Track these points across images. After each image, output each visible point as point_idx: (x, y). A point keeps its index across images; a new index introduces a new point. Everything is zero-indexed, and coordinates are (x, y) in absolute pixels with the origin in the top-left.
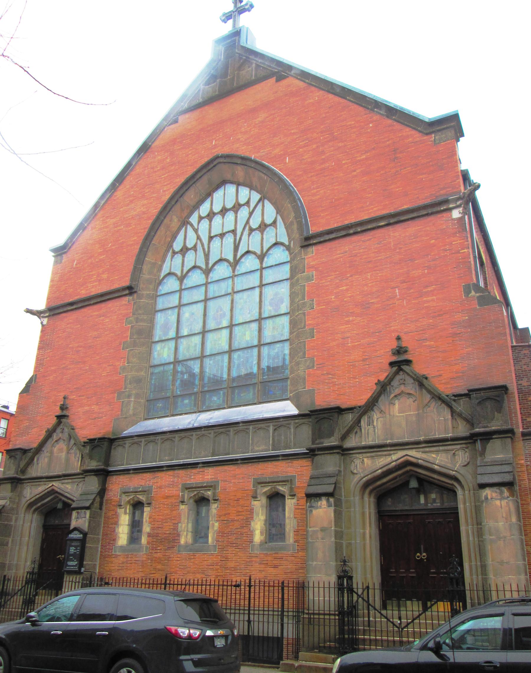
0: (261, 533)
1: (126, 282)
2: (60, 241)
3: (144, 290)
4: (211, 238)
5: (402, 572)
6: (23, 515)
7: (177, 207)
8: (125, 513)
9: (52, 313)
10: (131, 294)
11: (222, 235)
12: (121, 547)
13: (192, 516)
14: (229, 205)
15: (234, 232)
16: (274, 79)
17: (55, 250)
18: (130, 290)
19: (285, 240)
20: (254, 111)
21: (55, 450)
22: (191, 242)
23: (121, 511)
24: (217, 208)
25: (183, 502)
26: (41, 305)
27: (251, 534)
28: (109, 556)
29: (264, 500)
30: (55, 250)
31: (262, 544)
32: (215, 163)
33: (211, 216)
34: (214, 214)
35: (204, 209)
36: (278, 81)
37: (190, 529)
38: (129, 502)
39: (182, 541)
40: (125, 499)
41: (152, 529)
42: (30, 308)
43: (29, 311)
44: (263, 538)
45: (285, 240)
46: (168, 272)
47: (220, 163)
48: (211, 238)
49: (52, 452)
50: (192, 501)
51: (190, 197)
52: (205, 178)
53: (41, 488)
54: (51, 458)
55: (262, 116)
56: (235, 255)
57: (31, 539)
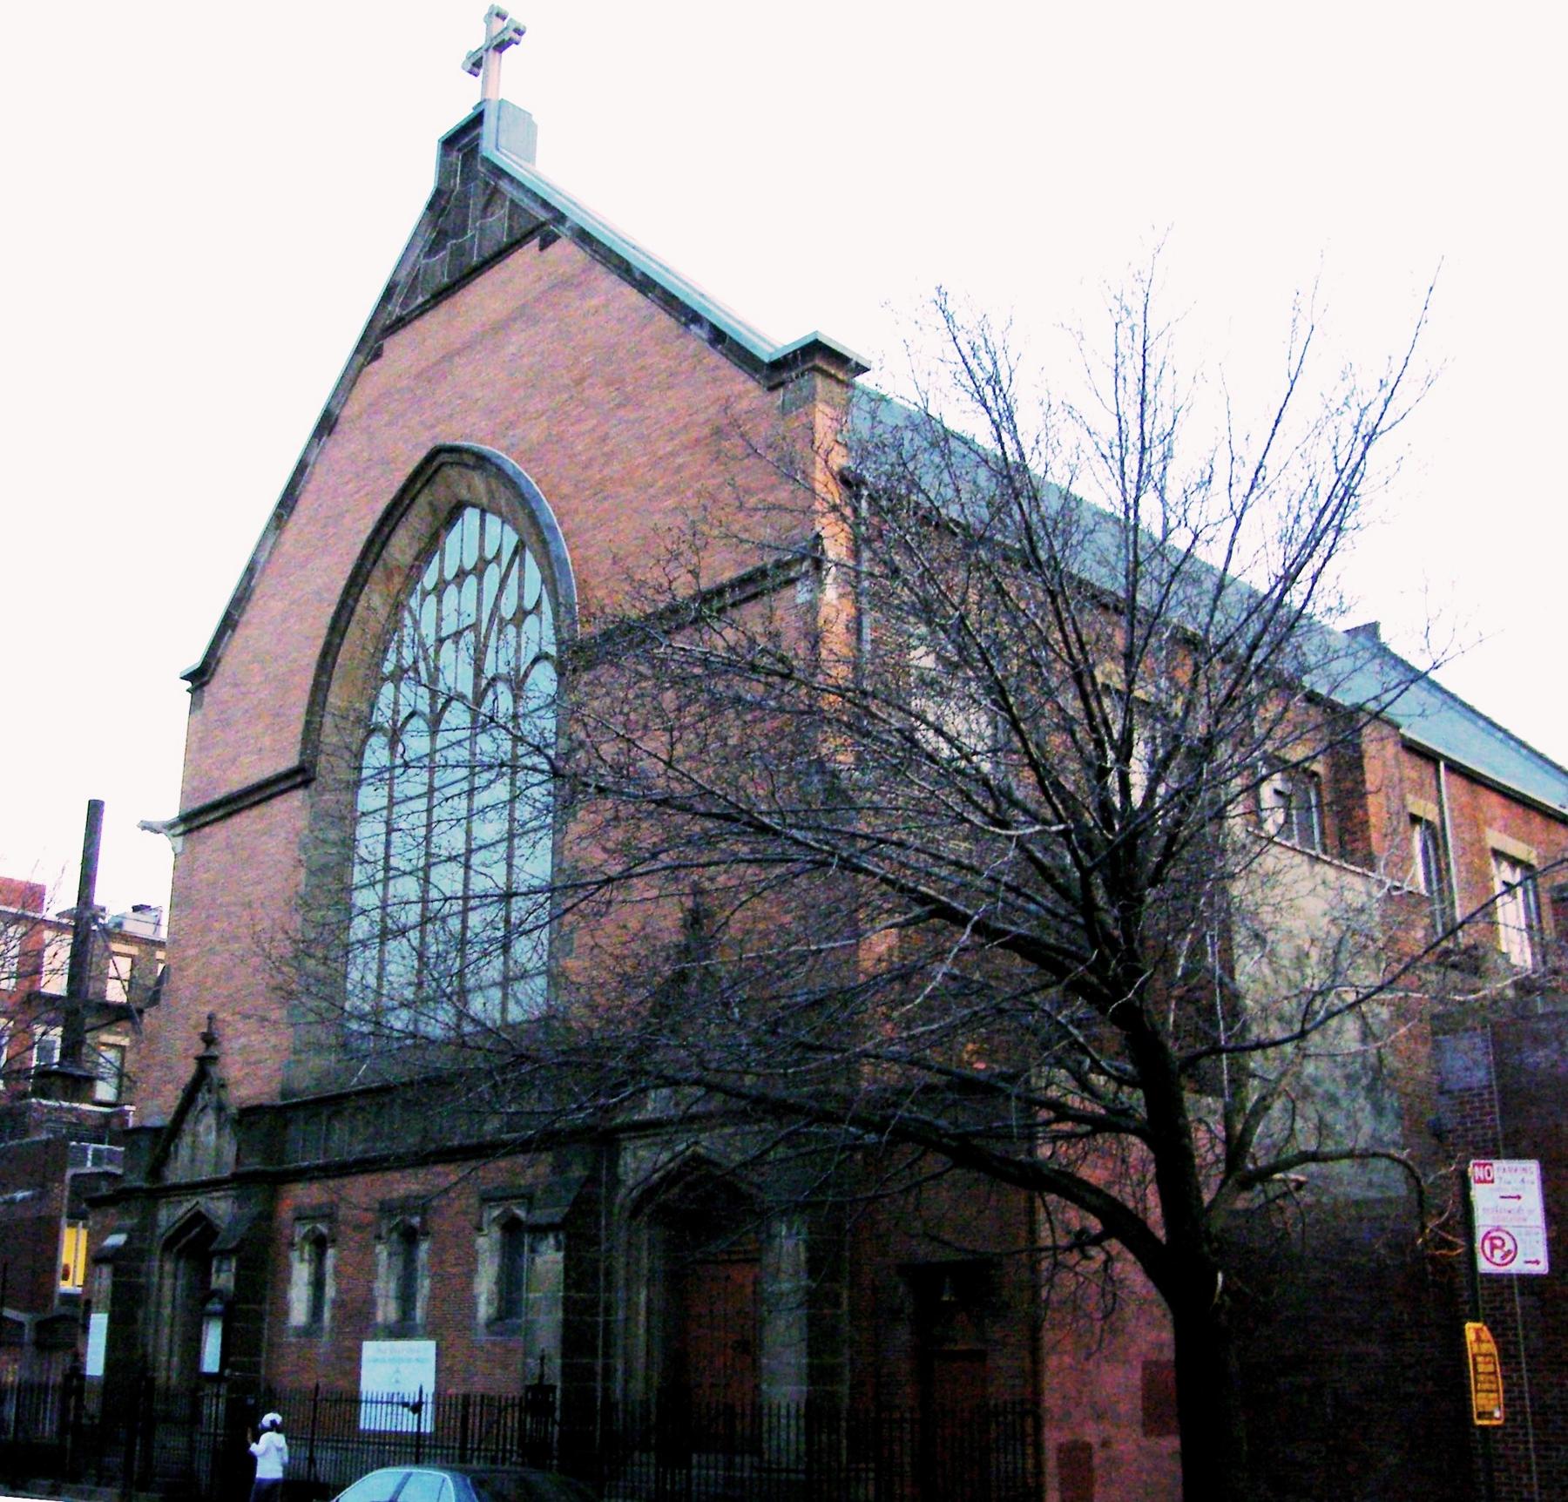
0: (489, 1302)
1: (290, 760)
2: (194, 660)
3: (330, 768)
4: (441, 641)
5: (1122, 804)
6: (156, 1264)
7: (378, 573)
8: (302, 1260)
9: (189, 825)
10: (305, 784)
11: (458, 634)
12: (296, 1328)
13: (398, 1263)
14: (469, 565)
15: (474, 627)
16: (536, 241)
17: (188, 677)
18: (300, 777)
19: (552, 650)
20: (502, 327)
21: (201, 1129)
22: (408, 656)
23: (295, 1255)
24: (449, 574)
25: (379, 1237)
26: (173, 813)
27: (472, 1302)
28: (280, 1345)
29: (496, 1232)
30: (188, 677)
31: (490, 1323)
32: (435, 464)
33: (440, 589)
34: (446, 583)
35: (429, 579)
36: (543, 247)
37: (392, 1293)
38: (305, 1238)
39: (380, 1318)
40: (302, 1229)
41: (339, 1291)
42: (149, 819)
43: (146, 827)
44: (492, 1311)
45: (552, 650)
46: (409, 710)
47: (442, 465)
48: (441, 641)
49: (195, 1135)
50: (395, 1236)
51: (402, 547)
52: (422, 500)
53: (184, 1207)
54: (194, 1146)
55: (516, 341)
56: (476, 685)
57: (179, 1311)
